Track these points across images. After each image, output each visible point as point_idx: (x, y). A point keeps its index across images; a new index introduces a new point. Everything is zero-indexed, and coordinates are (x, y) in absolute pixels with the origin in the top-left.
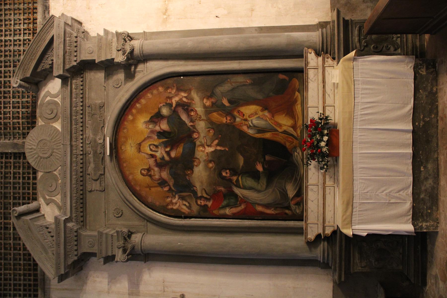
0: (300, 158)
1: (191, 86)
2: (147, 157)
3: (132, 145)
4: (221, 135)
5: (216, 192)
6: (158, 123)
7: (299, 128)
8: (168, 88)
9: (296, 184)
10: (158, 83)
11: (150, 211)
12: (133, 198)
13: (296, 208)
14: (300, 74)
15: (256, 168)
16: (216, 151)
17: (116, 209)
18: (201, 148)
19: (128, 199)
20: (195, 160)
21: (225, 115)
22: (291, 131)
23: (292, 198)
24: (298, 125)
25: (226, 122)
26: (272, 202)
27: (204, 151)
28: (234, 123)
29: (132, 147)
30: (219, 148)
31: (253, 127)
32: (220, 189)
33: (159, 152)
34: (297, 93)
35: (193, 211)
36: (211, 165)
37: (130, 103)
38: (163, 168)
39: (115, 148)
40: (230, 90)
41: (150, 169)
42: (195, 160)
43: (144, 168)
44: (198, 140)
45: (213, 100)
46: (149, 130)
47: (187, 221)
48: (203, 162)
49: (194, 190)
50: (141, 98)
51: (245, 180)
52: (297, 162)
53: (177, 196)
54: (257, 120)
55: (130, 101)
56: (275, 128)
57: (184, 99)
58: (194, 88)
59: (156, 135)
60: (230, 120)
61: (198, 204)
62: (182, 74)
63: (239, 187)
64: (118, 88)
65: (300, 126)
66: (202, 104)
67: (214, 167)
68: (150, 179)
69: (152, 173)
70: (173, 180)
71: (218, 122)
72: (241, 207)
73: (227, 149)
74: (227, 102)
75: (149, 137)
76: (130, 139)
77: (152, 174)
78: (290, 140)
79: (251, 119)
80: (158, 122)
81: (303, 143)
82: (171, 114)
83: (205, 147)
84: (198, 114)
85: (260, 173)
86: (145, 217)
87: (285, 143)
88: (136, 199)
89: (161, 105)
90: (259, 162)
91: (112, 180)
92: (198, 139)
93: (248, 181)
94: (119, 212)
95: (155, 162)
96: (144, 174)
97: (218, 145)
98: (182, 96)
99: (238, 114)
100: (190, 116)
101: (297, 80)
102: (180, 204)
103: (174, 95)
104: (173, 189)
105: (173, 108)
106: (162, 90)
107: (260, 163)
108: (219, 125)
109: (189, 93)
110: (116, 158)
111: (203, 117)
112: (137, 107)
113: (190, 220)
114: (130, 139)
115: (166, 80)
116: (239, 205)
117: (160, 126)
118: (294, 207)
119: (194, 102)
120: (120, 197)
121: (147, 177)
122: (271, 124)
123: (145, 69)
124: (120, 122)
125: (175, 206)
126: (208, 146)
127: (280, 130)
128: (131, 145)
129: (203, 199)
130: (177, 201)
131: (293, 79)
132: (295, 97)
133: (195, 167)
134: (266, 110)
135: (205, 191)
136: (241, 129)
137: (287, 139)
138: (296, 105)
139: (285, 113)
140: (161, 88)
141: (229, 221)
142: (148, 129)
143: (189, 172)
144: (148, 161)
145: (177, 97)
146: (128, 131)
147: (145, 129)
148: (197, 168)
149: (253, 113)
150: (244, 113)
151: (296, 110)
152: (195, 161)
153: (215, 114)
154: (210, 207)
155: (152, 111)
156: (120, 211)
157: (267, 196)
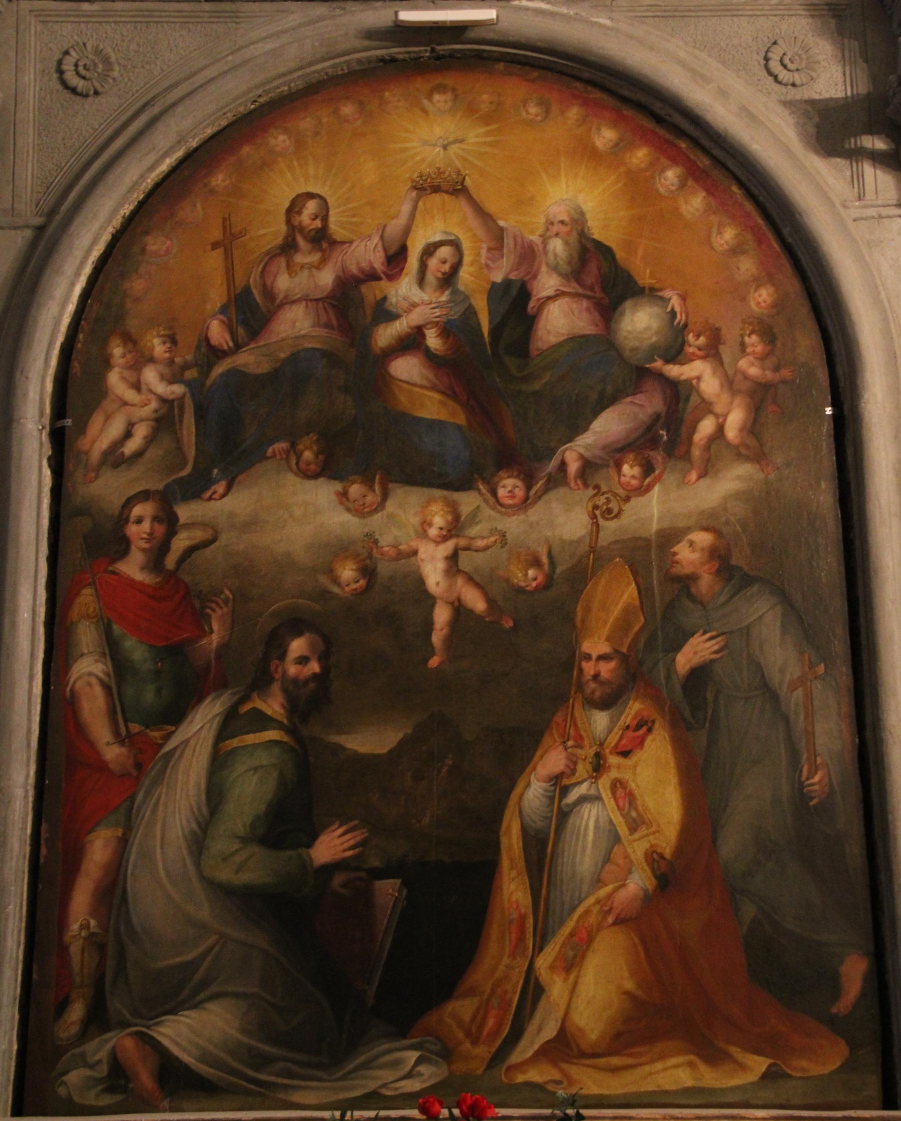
0: (384, 1086)
1: (779, 459)
2: (389, 230)
3: (455, 148)
4: (515, 628)
5: (197, 604)
6: (574, 287)
7: (556, 1075)
8: (768, 334)
9: (235, 1064)
10: (793, 285)
11: (95, 242)
12: (166, 154)
13: (91, 1067)
14: (872, 1085)
15: (331, 823)
16: (426, 600)
17: (106, 61)
18: (439, 521)
19: (160, 127)
20: (377, 487)
21: (624, 650)
22: (540, 1030)
23: (152, 1038)
24: (575, 1071)
25: (588, 657)
26: (135, 920)
27: (423, 534)
28: (580, 697)
29: (445, 148)
30: (442, 616)
31: (559, 808)
32: (216, 626)
33: (416, 294)
34: (759, 1064)
35: (96, 477)
36: (347, 572)
37: (682, 133)
38: (333, 318)
39: (439, 58)
40: (763, 675)
41: (325, 245)
42: (377, 487)
43: (332, 212)
44: (486, 501)
45: (706, 583)
46: (535, 238)
47: (36, 445)
48: (367, 530)
49: (209, 482)
50: (711, 191)
51: (265, 763)
52: (366, 1066)
53: (178, 389)
54: (596, 827)
55: (696, 133)
56: (554, 934)
57: (706, 426)
58: (772, 476)
59: (512, 277)
60: (596, 677)
61: (129, 503)
62: (846, 407)
63: (221, 736)
64: (766, 67)
65: (571, 1082)
66: (681, 524)
67: (336, 590)
68: (274, 243)
69: (305, 256)
70: (265, 368)
71: (588, 609)
72: (108, 744)
73: (434, 662)
74: (697, 660)
75: (498, 237)
76: (488, 134)
77: (299, 259)
78: (491, 1023)
79: (606, 795)
80: (582, 285)
81: (469, 1102)
82: (627, 354)
83: (445, 539)
84: (627, 499)
85: (303, 851)
86: (58, 218)
87: (472, 992)
88: (165, 167)
89: (675, 302)
90: (362, 844)
91: (262, 40)
92: (492, 500)
93: (255, 779)
94: (88, 75)
95: (362, 270)
96: (300, 213)
97: (459, 610)
98: (726, 416)
99: (628, 721)
100: (618, 456)
101: (841, 1066)
102: (133, 405)
103: (730, 372)
104: (219, 370)
105: (658, 364)
106: (758, 304)
107: (357, 851)
108: (569, 619)
109: (743, 451)
110: (382, 60)
111: (610, 528)
112: (663, 170)
113: (45, 463)
114: (488, 139)
115: (811, 324)
116: (123, 732)
117: (559, 295)
118: (97, 1057)
119: (694, 476)
120: (176, 85)
121: (284, 228)
122: (580, 910)
123: (871, 212)
124: (578, 84)
125: (123, 379)
126: (453, 559)
127: (543, 962)
128: (457, 141)
129: (160, 529)
130: (151, 391)
131: (843, 1042)
132: (733, 1050)
133: (338, 486)
134: (654, 882)
135: (205, 544)
136: (547, 740)
137: (495, 1001)
138: (692, 1057)
139: (640, 993)
140: (769, 300)
141: (31, 678)
142: (540, 231)
143: (308, 455)
144: (370, 237)
145: (722, 386)
146: (531, 123)
147: (542, 220)
148: (334, 498)
149: (639, 803)
150: (639, 756)
151: (662, 1057)
152: (371, 488)
153: (629, 593)
154: (114, 573)
155: (640, 252)
156: (97, 84)
157: (169, 887)
